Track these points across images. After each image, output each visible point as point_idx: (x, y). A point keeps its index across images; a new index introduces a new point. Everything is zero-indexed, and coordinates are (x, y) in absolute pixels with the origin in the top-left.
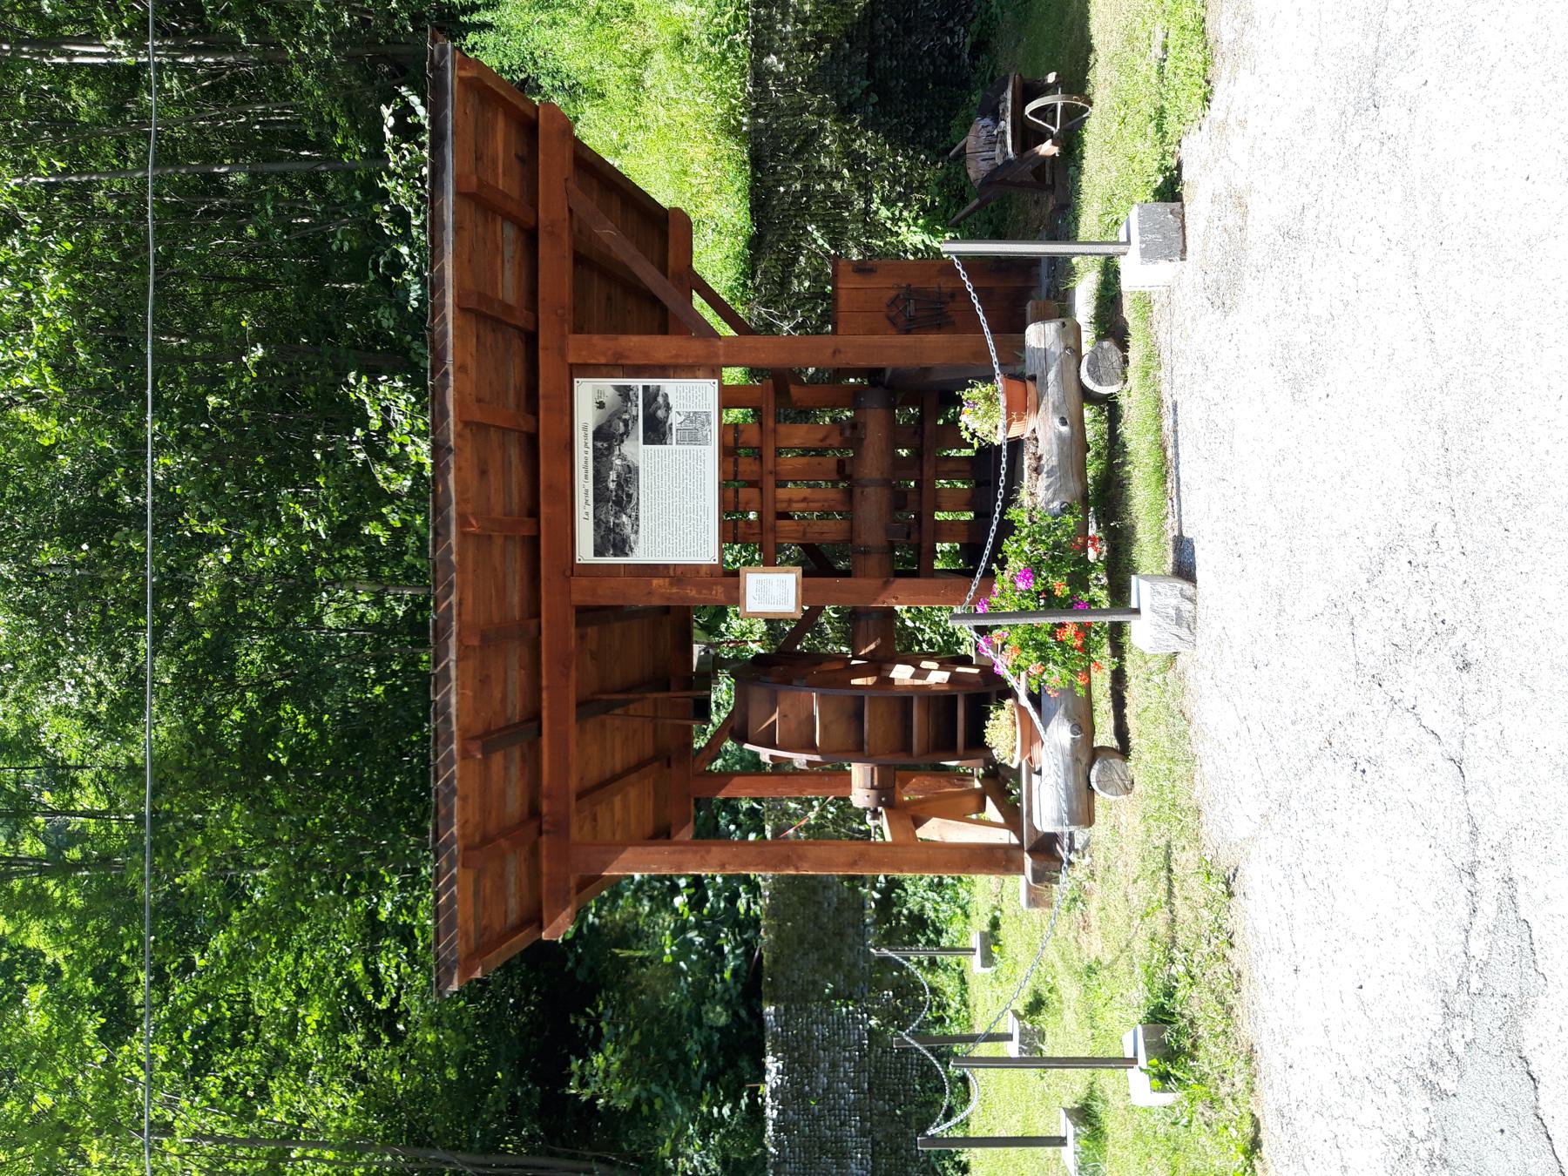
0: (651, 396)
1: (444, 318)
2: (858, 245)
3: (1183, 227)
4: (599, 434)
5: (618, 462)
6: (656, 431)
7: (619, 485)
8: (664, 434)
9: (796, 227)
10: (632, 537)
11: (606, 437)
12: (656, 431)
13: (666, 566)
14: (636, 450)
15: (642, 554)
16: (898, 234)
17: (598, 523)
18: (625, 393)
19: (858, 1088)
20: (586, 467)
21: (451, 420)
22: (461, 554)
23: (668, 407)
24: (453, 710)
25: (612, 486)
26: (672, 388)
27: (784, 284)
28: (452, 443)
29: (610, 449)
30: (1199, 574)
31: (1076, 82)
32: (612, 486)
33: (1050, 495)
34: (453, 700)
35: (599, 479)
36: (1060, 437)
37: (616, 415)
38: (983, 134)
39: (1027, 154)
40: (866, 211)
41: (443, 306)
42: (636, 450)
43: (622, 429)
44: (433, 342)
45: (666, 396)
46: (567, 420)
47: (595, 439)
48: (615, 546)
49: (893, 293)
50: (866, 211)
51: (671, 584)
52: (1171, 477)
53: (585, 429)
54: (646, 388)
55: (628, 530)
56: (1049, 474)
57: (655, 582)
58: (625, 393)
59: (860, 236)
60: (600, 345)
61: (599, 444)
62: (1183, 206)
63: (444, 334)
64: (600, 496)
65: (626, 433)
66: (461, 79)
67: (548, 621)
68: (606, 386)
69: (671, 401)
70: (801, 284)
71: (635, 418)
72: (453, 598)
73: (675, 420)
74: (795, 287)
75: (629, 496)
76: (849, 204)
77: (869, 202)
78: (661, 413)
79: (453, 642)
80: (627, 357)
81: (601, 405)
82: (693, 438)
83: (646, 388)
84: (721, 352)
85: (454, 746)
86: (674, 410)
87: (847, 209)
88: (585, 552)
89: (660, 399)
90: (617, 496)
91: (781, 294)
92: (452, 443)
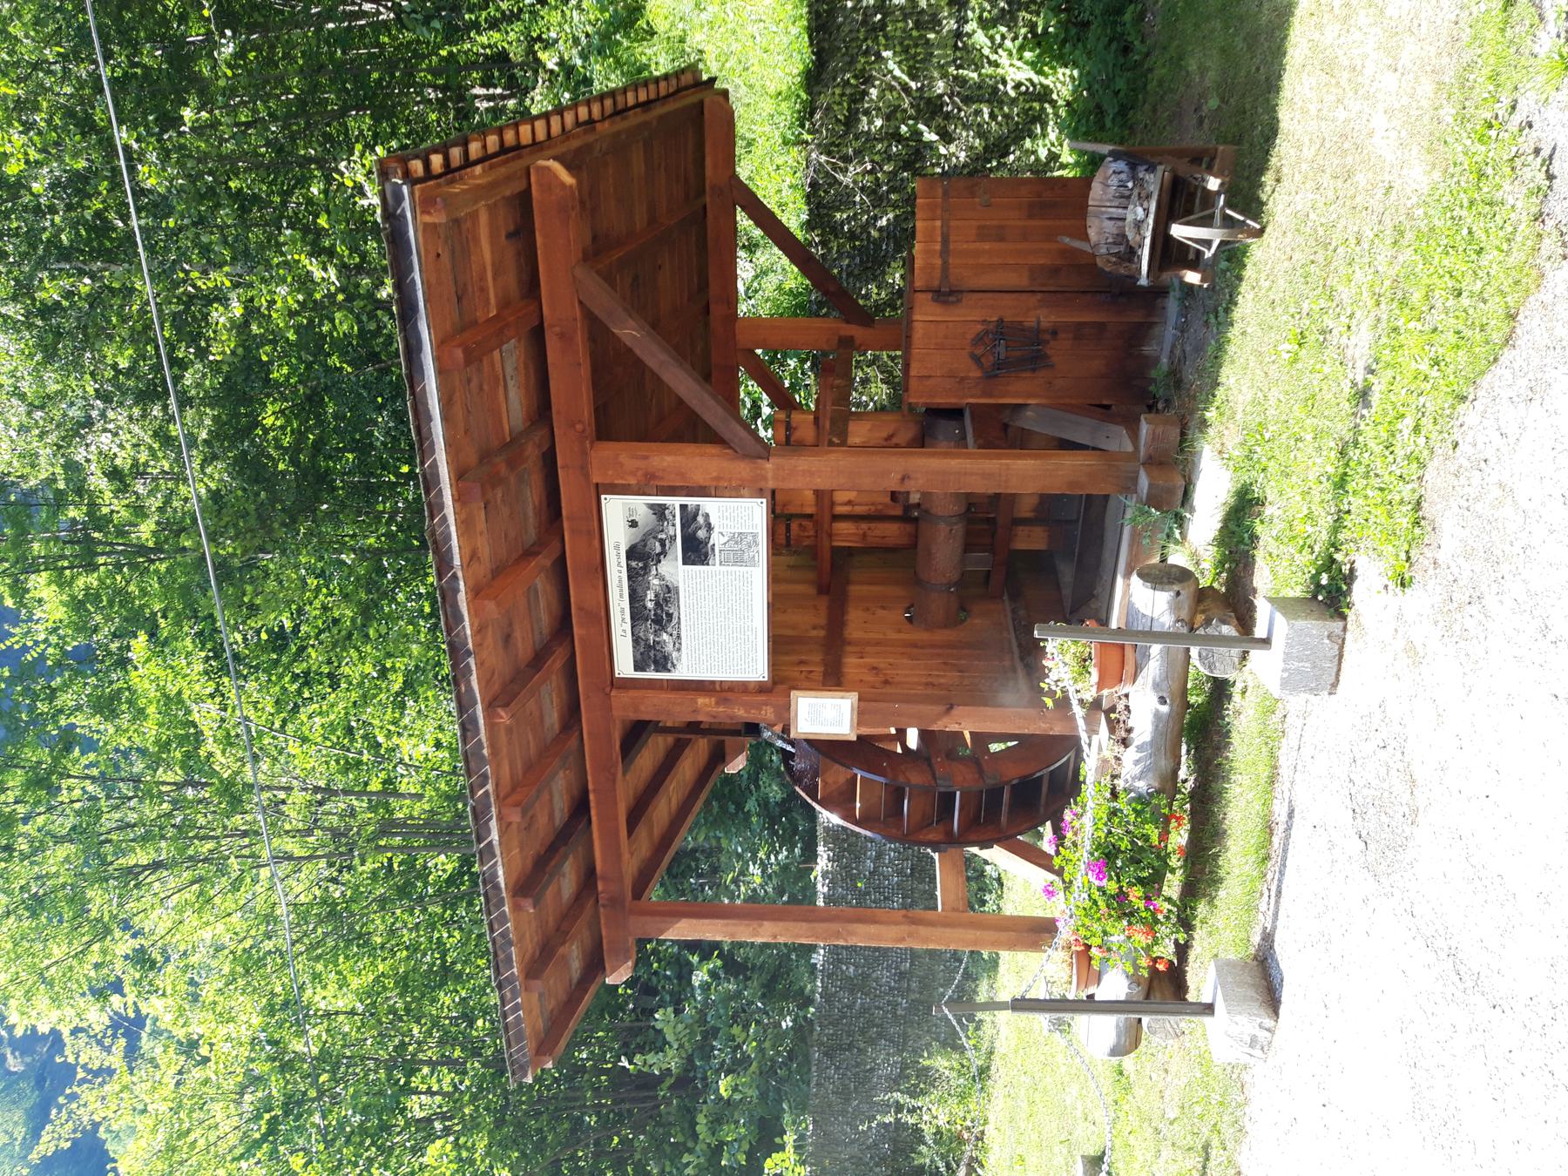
0: (689, 517)
1: (444, 519)
2: (944, 76)
3: (1341, 656)
4: (632, 553)
5: (656, 582)
6: (696, 551)
7: (658, 604)
8: (706, 555)
9: (867, 53)
10: (675, 654)
11: (641, 557)
12: (696, 551)
13: (713, 682)
14: (673, 569)
15: (686, 669)
16: (997, 65)
17: (636, 641)
18: (660, 512)
19: (900, 873)
20: (620, 586)
21: (467, 623)
22: (492, 745)
23: (709, 527)
24: (501, 880)
25: (650, 605)
26: (710, 506)
27: (851, 121)
28: (470, 645)
29: (646, 569)
30: (1283, 1010)
31: (1247, 199)
32: (650, 605)
33: (1137, 770)
34: (500, 872)
35: (635, 598)
36: (1157, 715)
37: (651, 534)
38: (1114, 181)
39: (1166, 276)
40: (958, 35)
41: (441, 507)
42: (673, 569)
43: (658, 549)
44: (435, 542)
45: (707, 516)
46: (596, 543)
47: (629, 557)
48: (656, 662)
49: (980, 327)
50: (958, 35)
51: (717, 703)
52: (1272, 867)
53: (617, 547)
54: (683, 507)
55: (669, 648)
56: (1140, 748)
57: (701, 701)
58: (660, 512)
59: (948, 64)
60: (626, 456)
61: (634, 564)
62: (1345, 629)
63: (448, 538)
64: (638, 614)
65: (664, 553)
66: (426, 225)
67: (589, 734)
68: (639, 505)
69: (713, 521)
70: (870, 122)
71: (673, 539)
72: (490, 787)
73: (717, 540)
74: (864, 125)
75: (670, 616)
76: (935, 23)
77: (963, 20)
78: (701, 534)
79: (493, 824)
80: (662, 478)
81: (633, 524)
82: (738, 559)
83: (683, 507)
84: (770, 475)
85: (506, 908)
86: (716, 530)
87: (933, 30)
88: (624, 665)
89: (700, 519)
90: (655, 615)
91: (846, 133)
92: (470, 645)
